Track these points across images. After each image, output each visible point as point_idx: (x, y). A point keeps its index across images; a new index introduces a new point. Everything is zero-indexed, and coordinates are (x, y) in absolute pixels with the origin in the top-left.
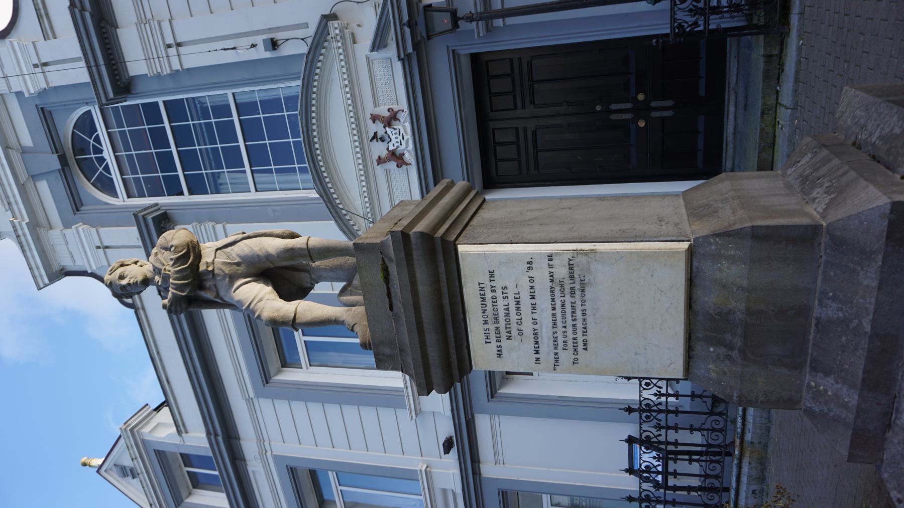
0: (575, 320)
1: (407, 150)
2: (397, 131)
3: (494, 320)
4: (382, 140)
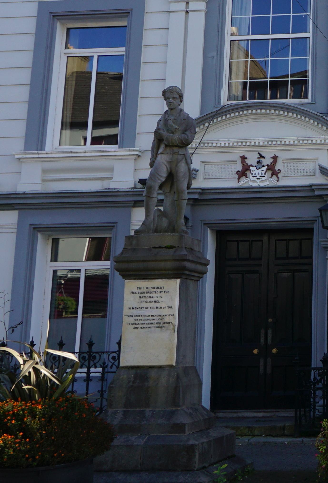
0: (147, 324)
1: (249, 180)
2: (263, 175)
3: (148, 291)
4: (259, 162)
